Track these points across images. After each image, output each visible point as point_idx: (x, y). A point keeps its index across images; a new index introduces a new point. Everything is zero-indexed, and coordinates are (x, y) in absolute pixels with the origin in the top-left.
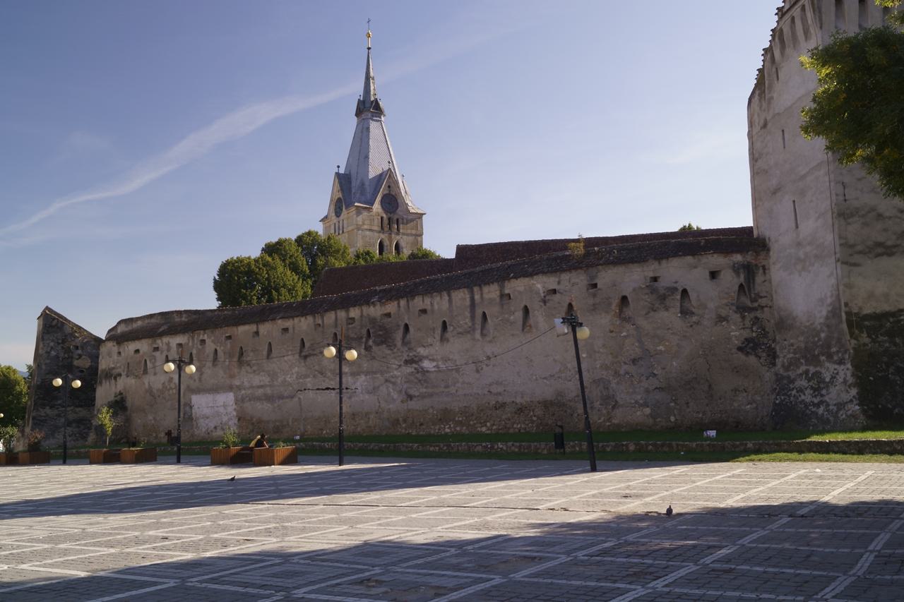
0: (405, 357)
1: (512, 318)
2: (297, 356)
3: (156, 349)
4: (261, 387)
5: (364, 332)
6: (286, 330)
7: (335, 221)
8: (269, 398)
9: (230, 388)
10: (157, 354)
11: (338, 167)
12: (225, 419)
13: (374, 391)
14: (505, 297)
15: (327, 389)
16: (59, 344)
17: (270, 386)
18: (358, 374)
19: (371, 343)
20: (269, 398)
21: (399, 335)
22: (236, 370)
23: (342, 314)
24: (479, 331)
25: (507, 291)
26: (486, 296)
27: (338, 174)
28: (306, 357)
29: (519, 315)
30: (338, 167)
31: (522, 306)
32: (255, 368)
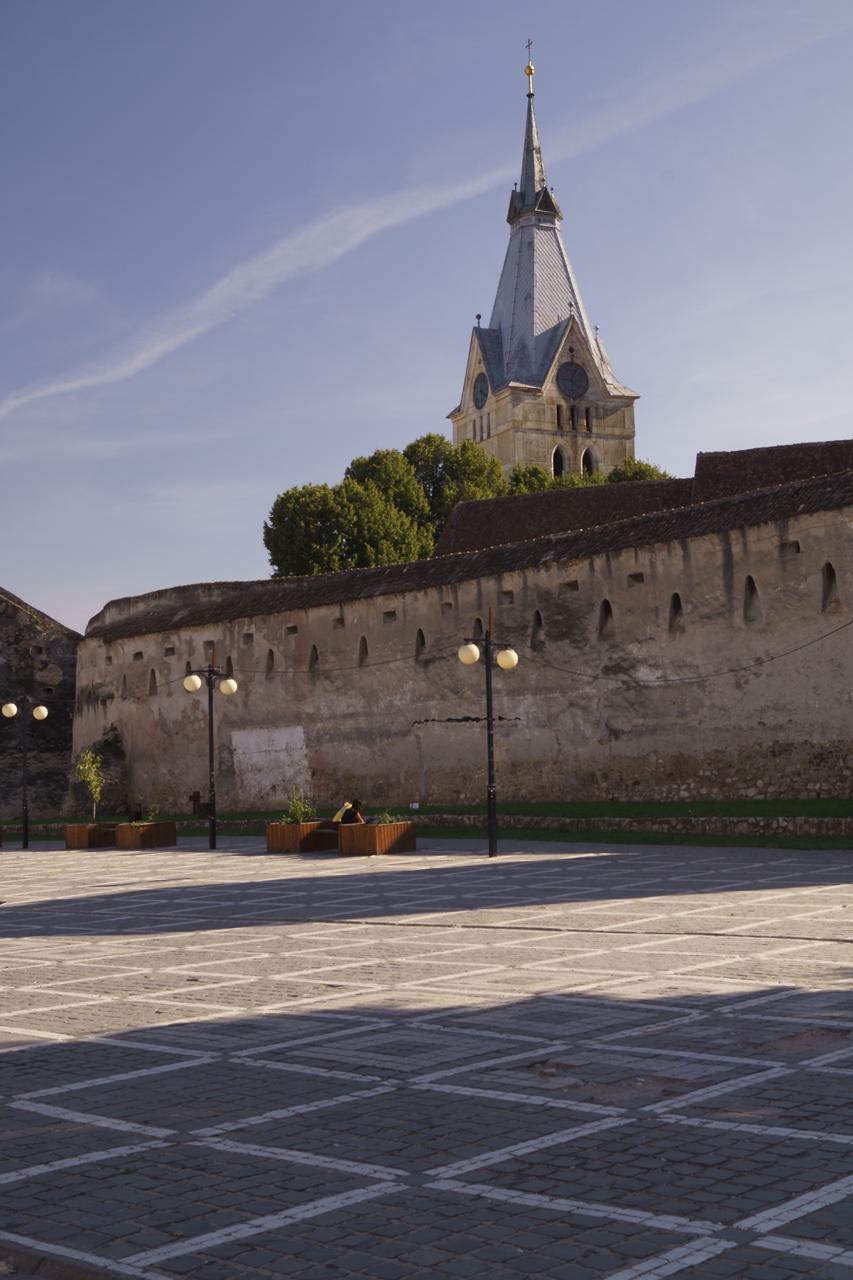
0: (605, 661)
1: (802, 587)
2: (411, 662)
3: (170, 651)
5: (530, 616)
6: (391, 615)
7: (474, 416)
8: (365, 737)
9: (297, 719)
10: (172, 660)
11: (479, 317)
12: (290, 772)
14: (790, 548)
15: (466, 719)
16: (9, 644)
17: (367, 715)
19: (542, 636)
21: (593, 621)
23: (489, 585)
24: (741, 612)
25: (792, 538)
26: (754, 547)
27: (477, 331)
28: (427, 663)
29: (816, 581)
30: (479, 317)
31: (822, 564)
32: (339, 683)
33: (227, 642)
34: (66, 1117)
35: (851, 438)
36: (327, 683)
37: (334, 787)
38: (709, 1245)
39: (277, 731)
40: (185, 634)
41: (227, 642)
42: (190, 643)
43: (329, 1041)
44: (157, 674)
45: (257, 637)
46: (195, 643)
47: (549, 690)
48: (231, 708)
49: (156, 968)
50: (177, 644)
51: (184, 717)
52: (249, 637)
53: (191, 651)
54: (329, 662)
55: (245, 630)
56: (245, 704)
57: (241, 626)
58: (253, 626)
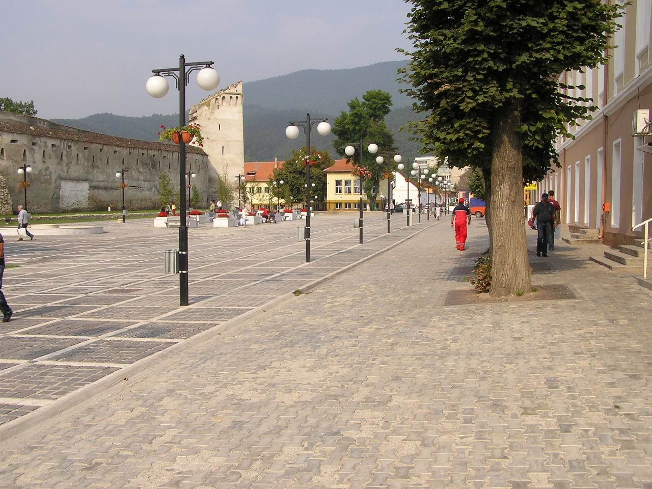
4: (103, 181)
6: (115, 152)
8: (106, 188)
9: (86, 180)
13: (150, 190)
15: (134, 186)
18: (146, 181)
20: (106, 188)
22: (91, 170)
32: (101, 170)
33: (62, 147)
34: (21, 404)
35: (179, 67)
36: (97, 170)
37: (95, 204)
38: (204, 403)
39: (78, 184)
40: (43, 139)
41: (62, 147)
42: (45, 143)
43: (137, 284)
44: (27, 153)
45: (73, 148)
46: (48, 144)
47: (151, 181)
48: (62, 173)
49: (573, 32)
50: (39, 142)
51: (39, 173)
52: (70, 147)
53: (46, 146)
54: (99, 163)
55: (69, 144)
56: (67, 172)
57: (68, 143)
58: (72, 143)
